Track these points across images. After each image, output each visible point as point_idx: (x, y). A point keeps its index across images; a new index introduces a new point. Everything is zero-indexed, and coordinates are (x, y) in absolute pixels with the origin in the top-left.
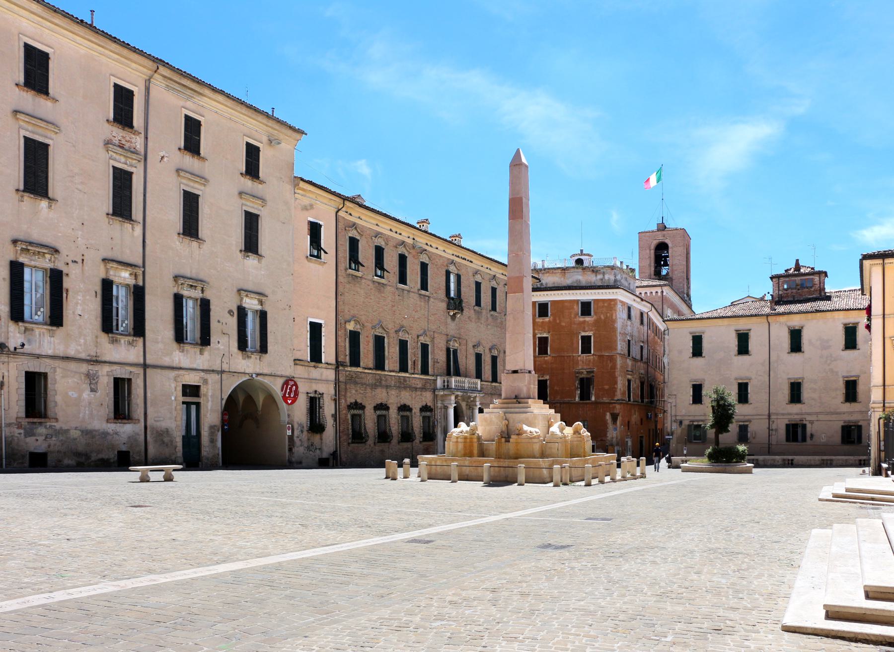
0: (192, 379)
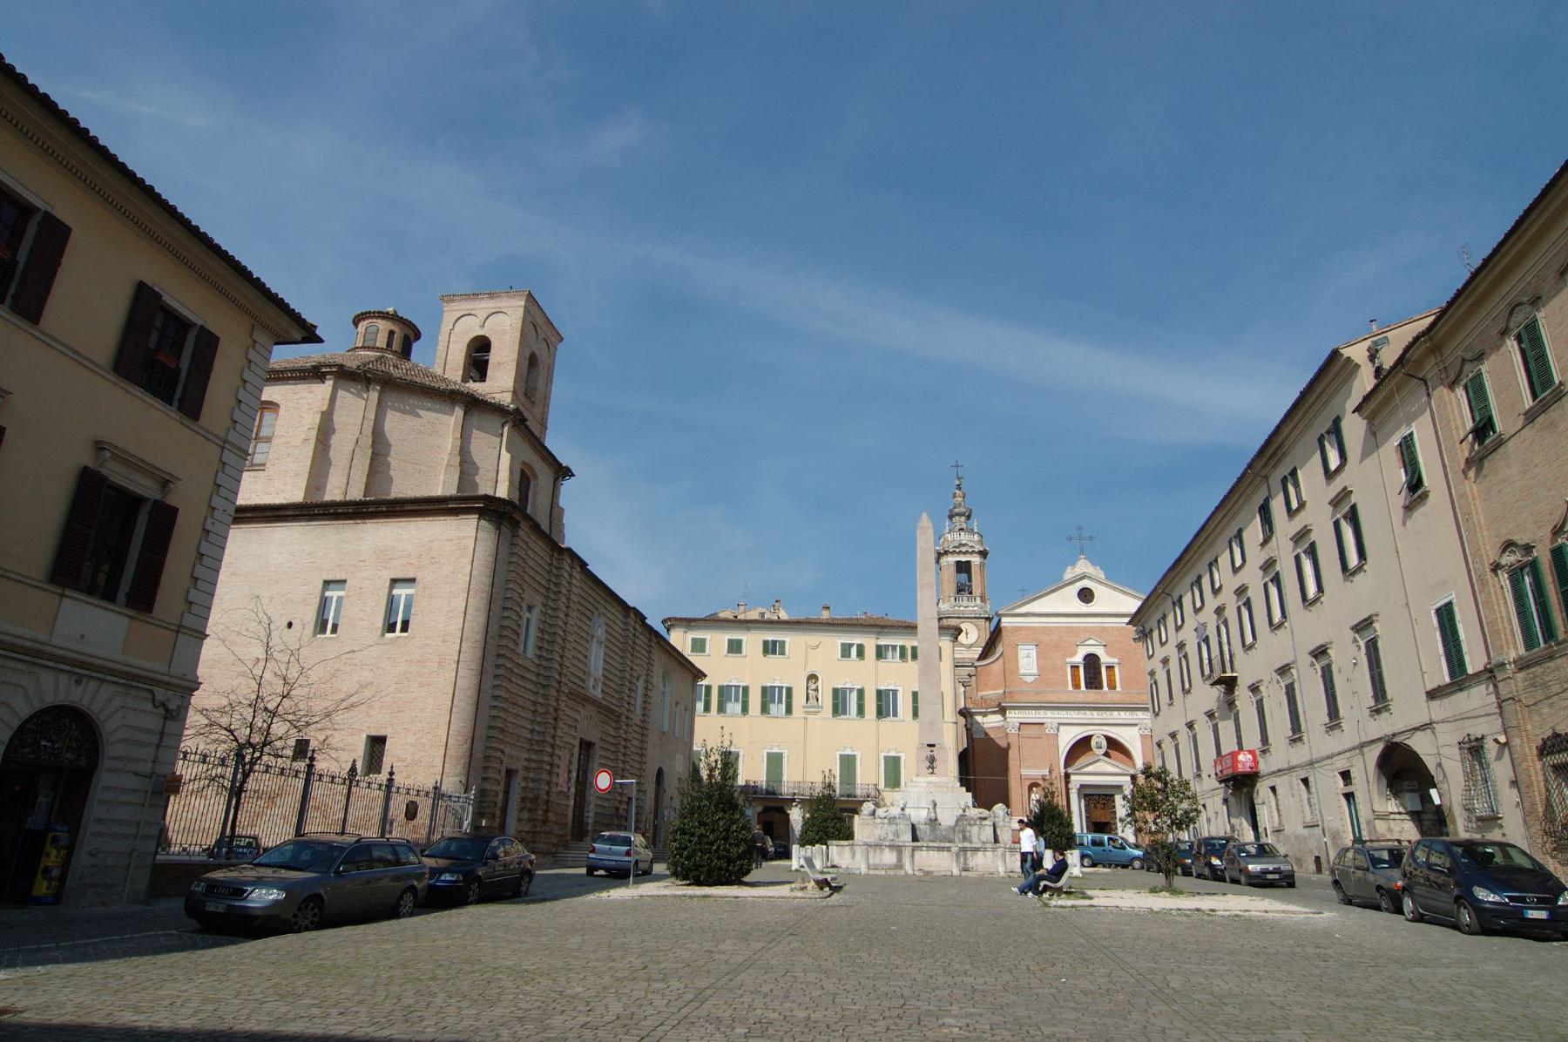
0: (1341, 764)
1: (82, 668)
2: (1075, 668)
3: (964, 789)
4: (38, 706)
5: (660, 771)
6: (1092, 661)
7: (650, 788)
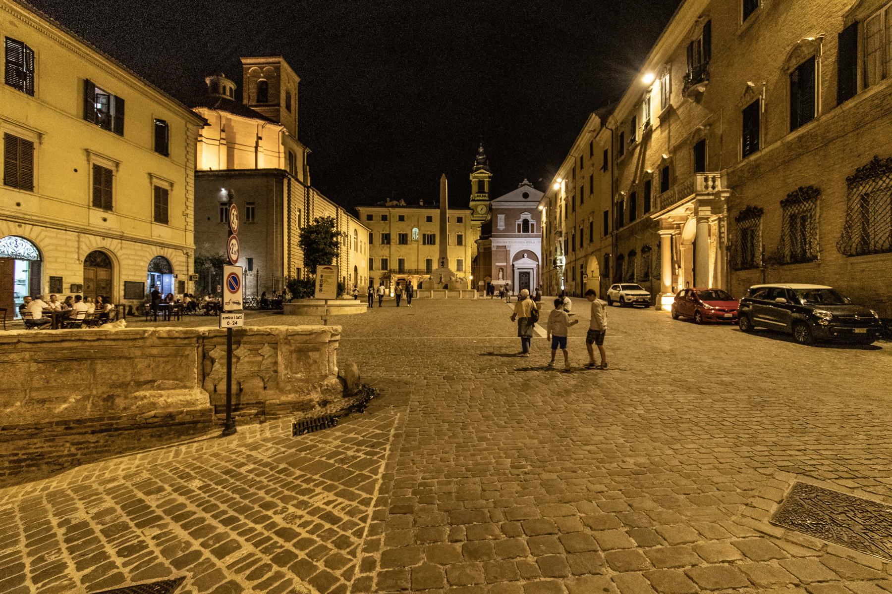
1: (162, 245)
2: (519, 225)
3: (759, 207)
4: (153, 256)
5: (356, 267)
6: (526, 222)
7: (352, 272)
